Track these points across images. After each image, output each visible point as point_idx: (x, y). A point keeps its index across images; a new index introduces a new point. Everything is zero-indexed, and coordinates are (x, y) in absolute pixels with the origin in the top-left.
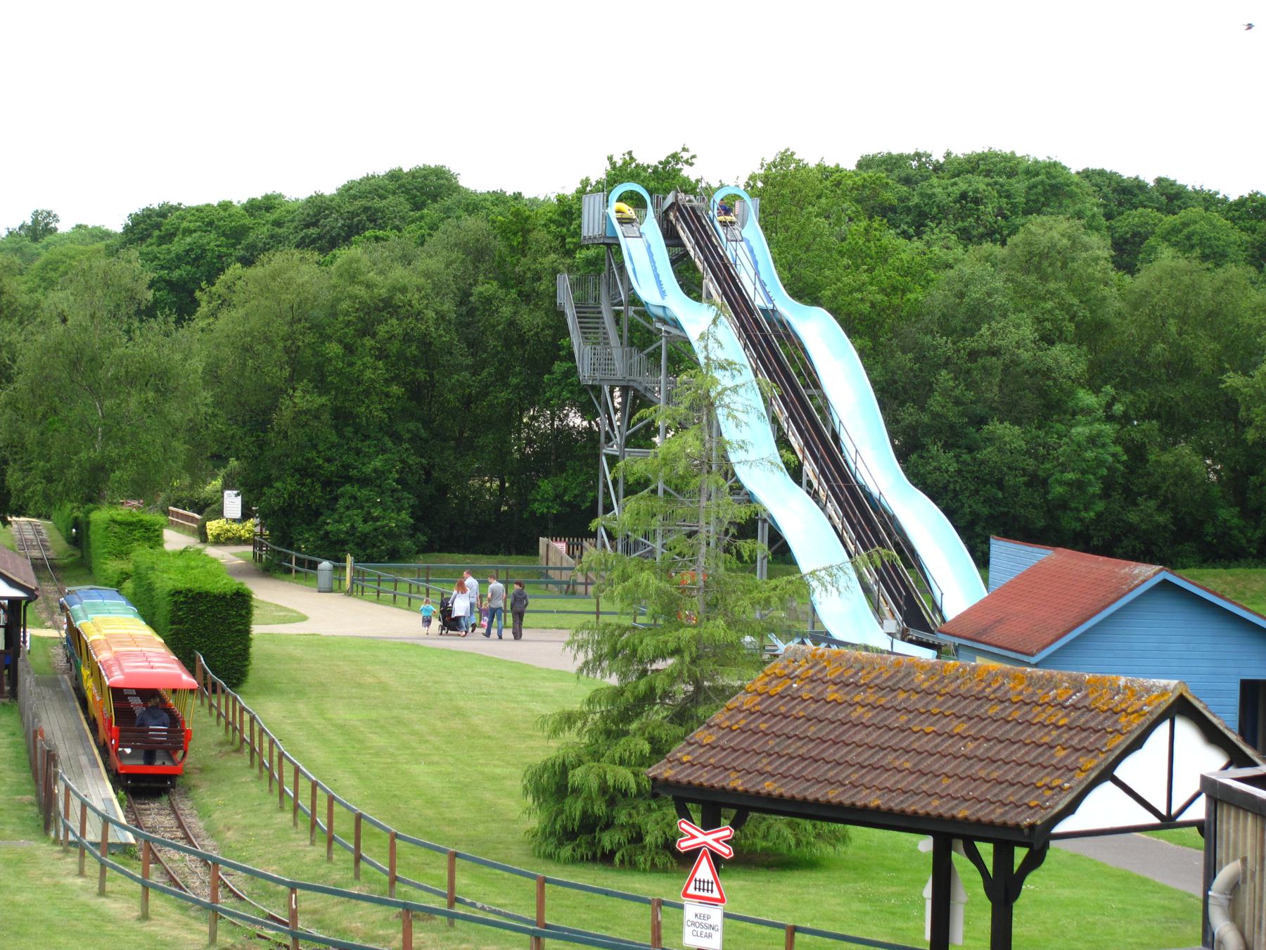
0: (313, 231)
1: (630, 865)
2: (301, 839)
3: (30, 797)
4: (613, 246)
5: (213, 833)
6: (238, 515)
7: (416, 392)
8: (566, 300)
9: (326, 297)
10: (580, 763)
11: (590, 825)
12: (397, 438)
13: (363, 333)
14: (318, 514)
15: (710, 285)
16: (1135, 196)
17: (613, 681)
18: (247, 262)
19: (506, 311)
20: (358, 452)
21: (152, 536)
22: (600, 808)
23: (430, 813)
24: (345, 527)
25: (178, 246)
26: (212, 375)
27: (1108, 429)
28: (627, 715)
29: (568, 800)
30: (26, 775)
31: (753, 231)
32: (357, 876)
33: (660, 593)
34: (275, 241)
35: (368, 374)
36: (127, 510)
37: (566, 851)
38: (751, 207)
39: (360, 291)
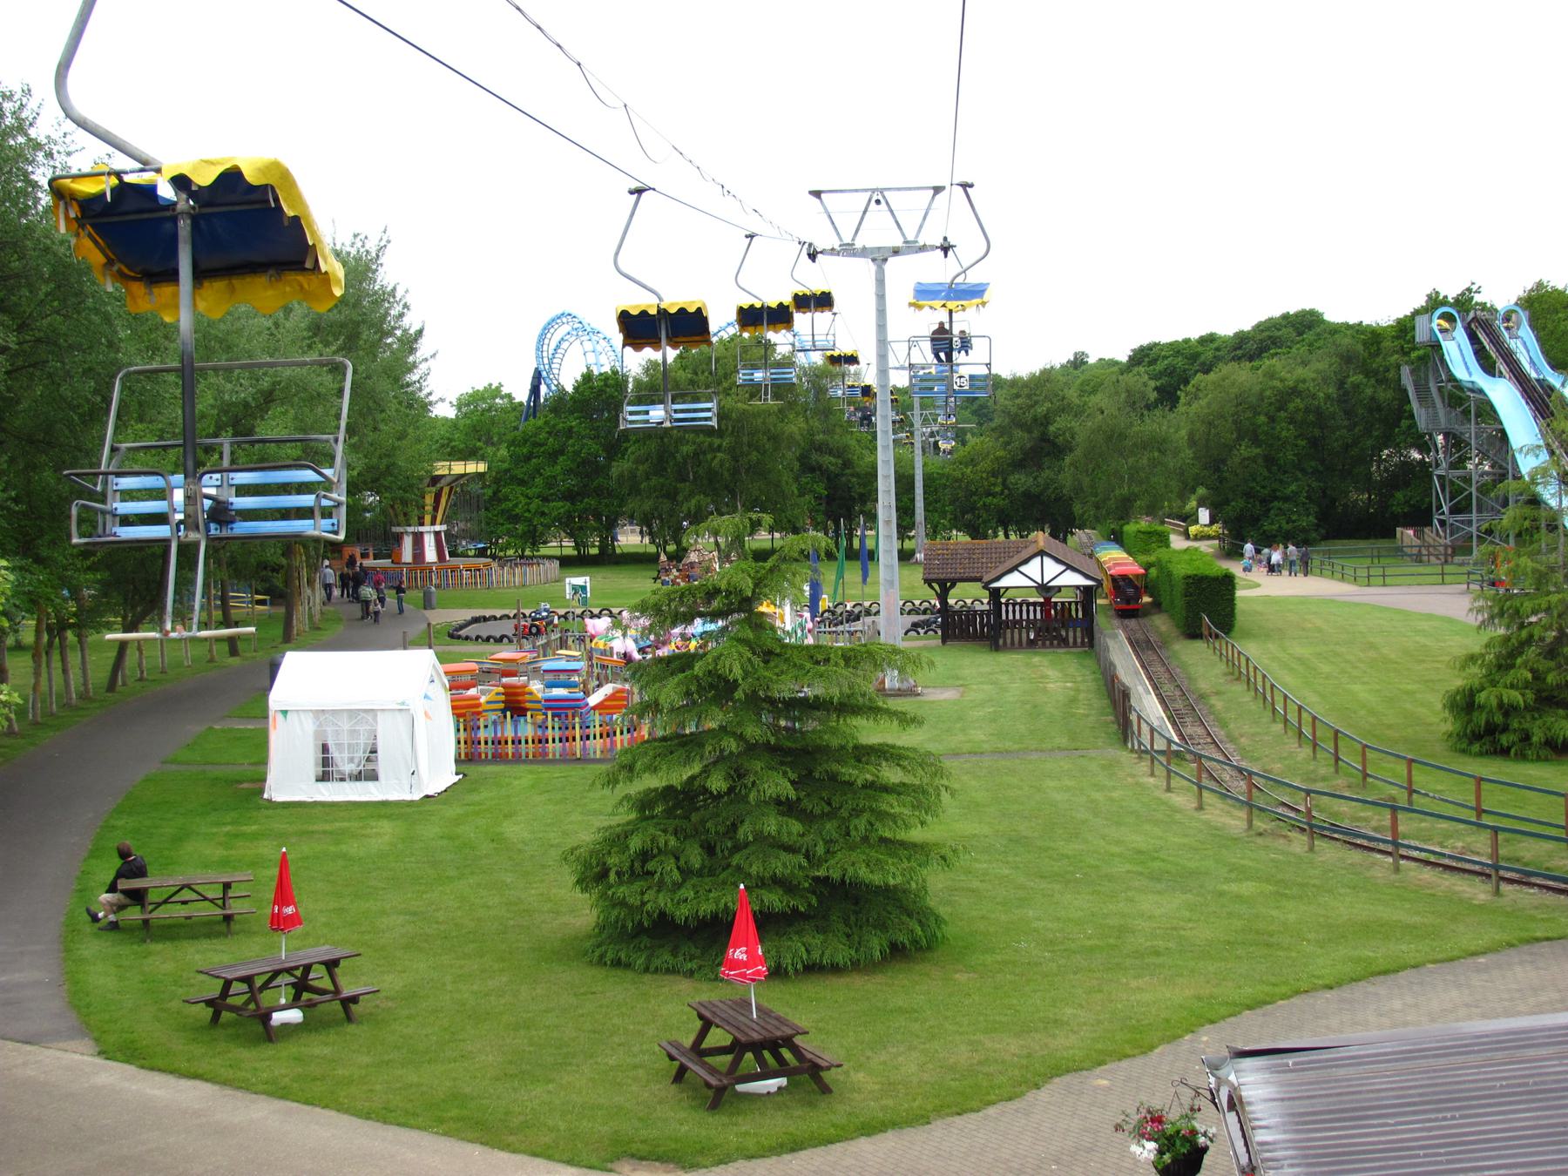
0: (1239, 352)
1: (1522, 757)
2: (1292, 744)
3: (1112, 718)
4: (1437, 347)
5: (1232, 739)
6: (1207, 521)
7: (1314, 443)
8: (1407, 380)
9: (1257, 388)
10: (1482, 689)
11: (1491, 730)
12: (1303, 471)
13: (1279, 409)
14: (1258, 519)
15: (1501, 366)
17: (1502, 631)
18: (1207, 372)
19: (1369, 391)
20: (1281, 481)
21: (1163, 540)
22: (1498, 719)
23: (1372, 720)
24: (1275, 527)
25: (1160, 366)
26: (1192, 441)
28: (1514, 653)
29: (1476, 714)
30: (1106, 702)
31: (1526, 332)
32: (1337, 771)
33: (1534, 571)
34: (1217, 359)
35: (1284, 433)
36: (1144, 524)
37: (1476, 747)
38: (1524, 316)
39: (1277, 383)
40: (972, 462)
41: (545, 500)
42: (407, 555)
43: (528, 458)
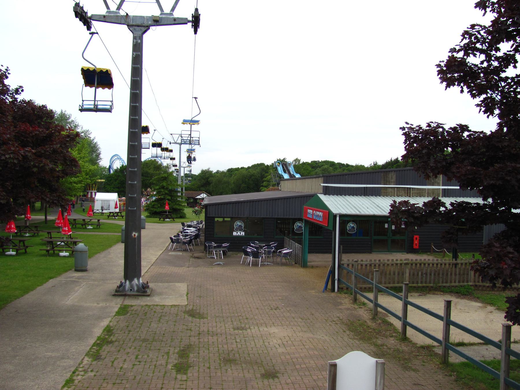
26: (234, 183)
40: (194, 185)
41: (114, 188)
42: (89, 196)
43: (111, 180)
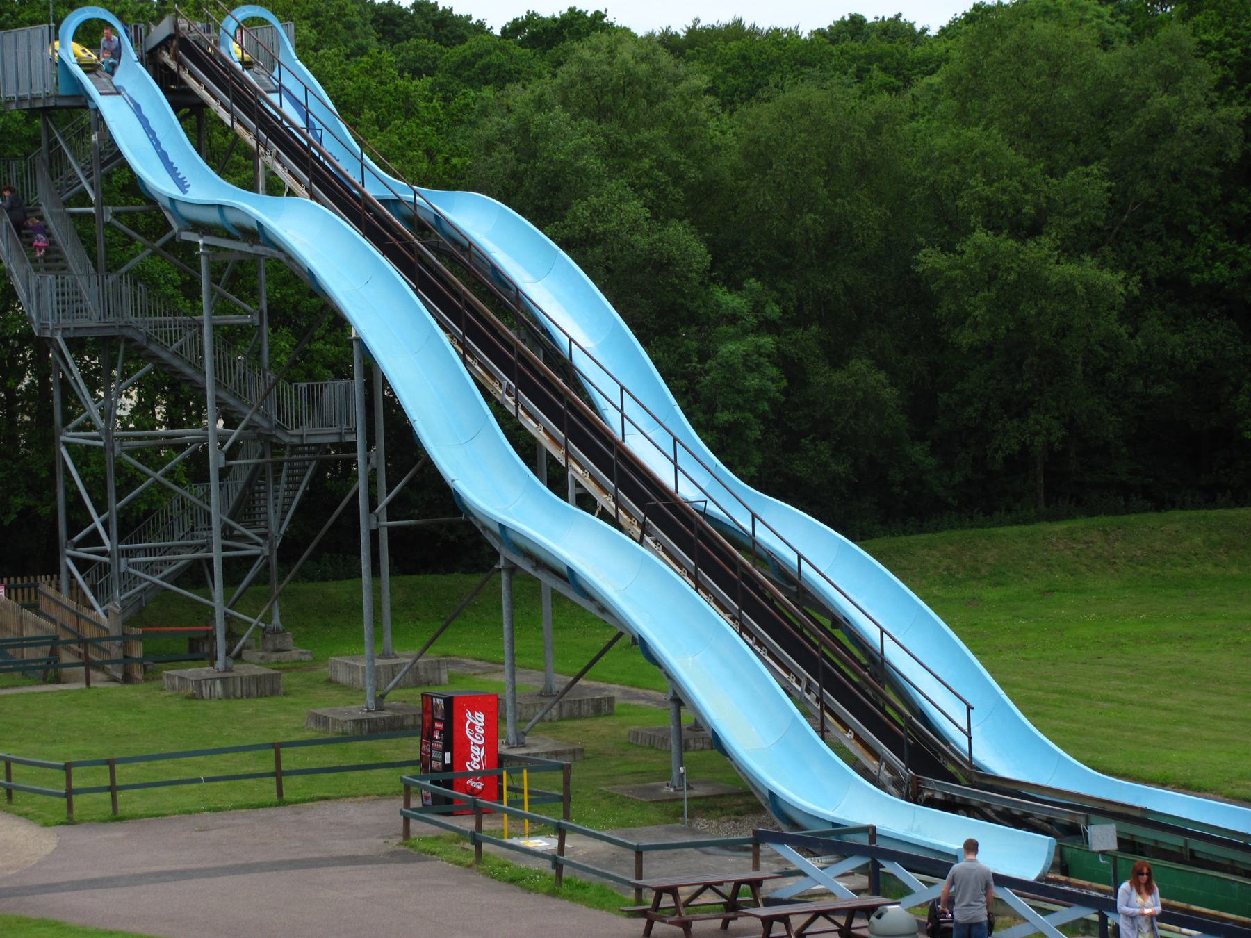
16: (398, 25)
27: (767, 341)
